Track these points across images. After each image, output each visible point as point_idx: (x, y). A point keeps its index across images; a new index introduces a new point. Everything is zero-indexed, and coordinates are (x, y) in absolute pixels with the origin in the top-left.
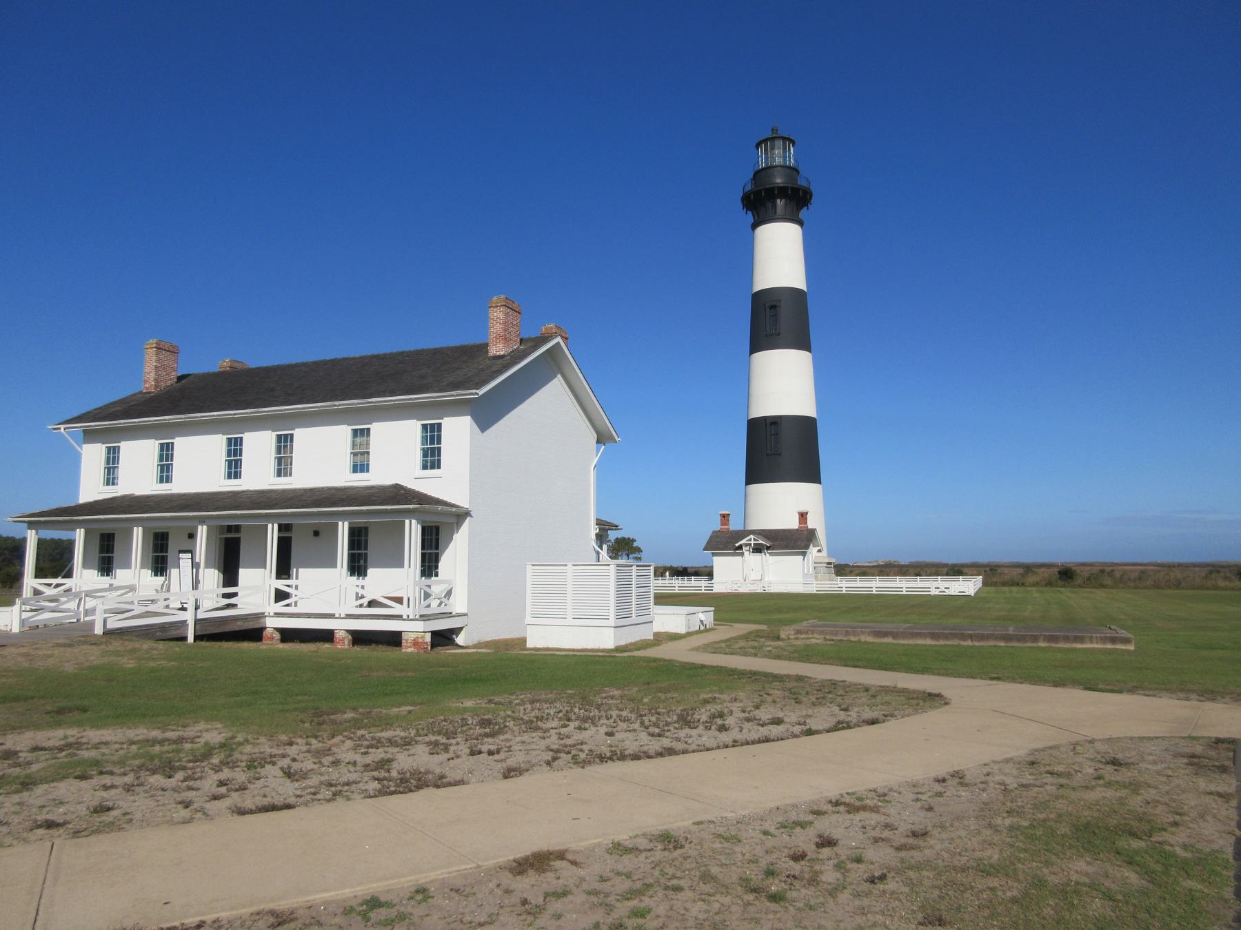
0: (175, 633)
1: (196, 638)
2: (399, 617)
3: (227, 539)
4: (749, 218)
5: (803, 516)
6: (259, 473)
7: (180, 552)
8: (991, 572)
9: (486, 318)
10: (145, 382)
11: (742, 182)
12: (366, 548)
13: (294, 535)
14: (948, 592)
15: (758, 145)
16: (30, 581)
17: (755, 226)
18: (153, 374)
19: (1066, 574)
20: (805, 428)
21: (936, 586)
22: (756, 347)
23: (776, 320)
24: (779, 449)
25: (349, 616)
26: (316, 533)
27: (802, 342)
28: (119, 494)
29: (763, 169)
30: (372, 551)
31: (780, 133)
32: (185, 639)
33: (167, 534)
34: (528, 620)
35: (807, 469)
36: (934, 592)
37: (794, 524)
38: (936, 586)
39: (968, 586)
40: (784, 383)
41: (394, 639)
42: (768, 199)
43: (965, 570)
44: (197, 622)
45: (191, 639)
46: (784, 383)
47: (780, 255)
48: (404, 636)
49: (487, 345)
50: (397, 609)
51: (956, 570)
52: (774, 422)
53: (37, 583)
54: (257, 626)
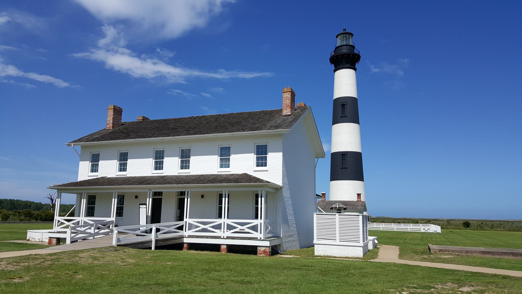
0: (146, 245)
1: (156, 248)
2: (219, 237)
3: (180, 198)
4: (333, 67)
5: (359, 195)
6: (172, 167)
7: (140, 204)
8: (447, 225)
9: (282, 97)
10: (107, 124)
11: (330, 52)
12: (94, 204)
13: (164, 198)
14: (429, 231)
15: (337, 37)
16: (57, 218)
17: (335, 71)
18: (111, 121)
19: (467, 224)
20: (357, 157)
21: (422, 228)
22: (335, 122)
23: (346, 111)
24: (347, 166)
25: (228, 238)
26: (136, 197)
27: (356, 120)
28: (99, 177)
29: (340, 46)
30: (97, 206)
31: (347, 31)
32: (151, 248)
33: (95, 196)
34: (315, 241)
35: (357, 174)
36: (423, 231)
37: (355, 199)
38: (422, 228)
39: (435, 229)
40: (345, 137)
41: (252, 250)
42: (345, 59)
43: (420, 222)
44: (157, 241)
45: (153, 248)
46: (345, 137)
47: (345, 83)
48: (259, 248)
49: (282, 110)
50: (255, 234)
51: (428, 221)
52: (344, 155)
53: (61, 219)
54: (180, 242)
